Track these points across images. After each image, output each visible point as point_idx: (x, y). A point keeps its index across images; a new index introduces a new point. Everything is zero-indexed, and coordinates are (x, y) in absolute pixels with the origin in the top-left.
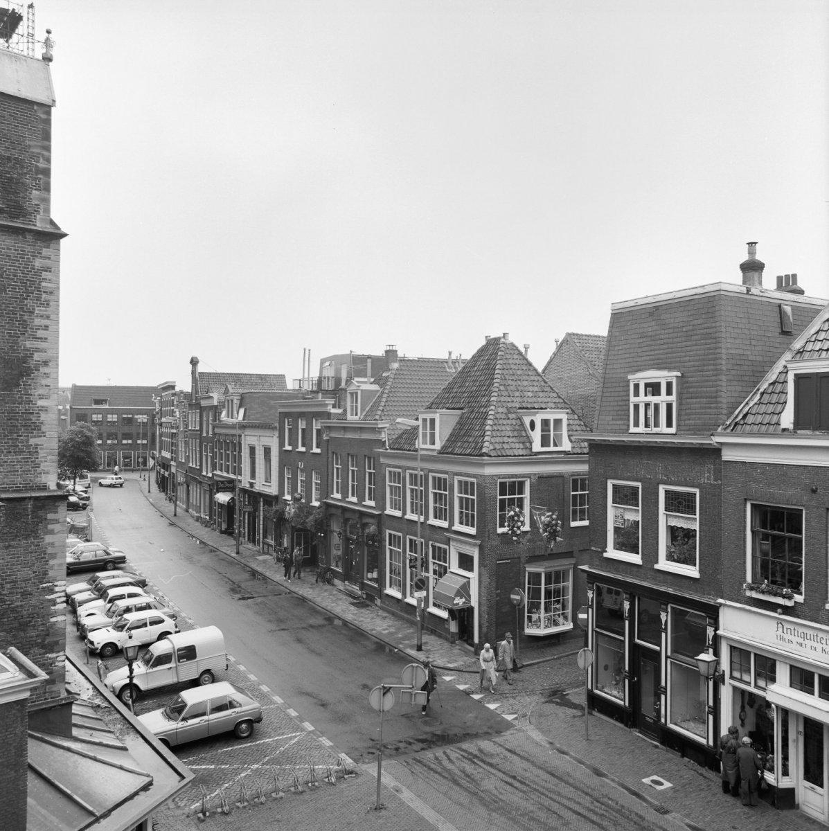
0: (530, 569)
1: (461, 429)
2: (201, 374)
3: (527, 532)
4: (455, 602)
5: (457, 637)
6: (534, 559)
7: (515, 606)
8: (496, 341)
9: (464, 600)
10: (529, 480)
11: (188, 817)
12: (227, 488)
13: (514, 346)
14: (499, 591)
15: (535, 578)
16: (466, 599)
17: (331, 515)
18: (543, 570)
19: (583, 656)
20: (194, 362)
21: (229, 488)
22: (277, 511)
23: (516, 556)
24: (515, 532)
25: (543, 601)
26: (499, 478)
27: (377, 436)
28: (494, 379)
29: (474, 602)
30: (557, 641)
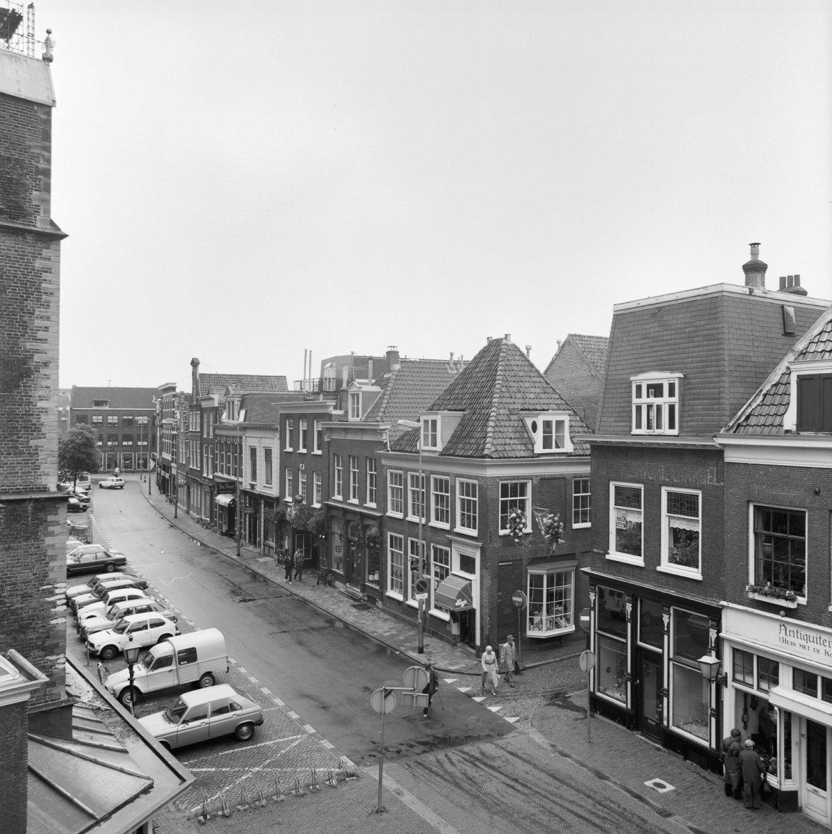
0: (532, 571)
1: (462, 431)
2: (202, 375)
3: (529, 534)
4: (456, 604)
5: (458, 640)
6: (536, 561)
7: (517, 608)
8: (498, 342)
9: (465, 602)
10: (531, 482)
11: (188, 819)
12: (228, 489)
13: (516, 347)
14: (501, 593)
15: (537, 580)
16: (468, 602)
17: (332, 517)
18: (545, 572)
19: (585, 658)
20: (195, 363)
21: (230, 490)
22: (278, 513)
23: (518, 558)
24: (517, 534)
25: (545, 603)
26: (501, 480)
27: (378, 437)
28: (495, 380)
29: (476, 605)
30: (559, 643)
